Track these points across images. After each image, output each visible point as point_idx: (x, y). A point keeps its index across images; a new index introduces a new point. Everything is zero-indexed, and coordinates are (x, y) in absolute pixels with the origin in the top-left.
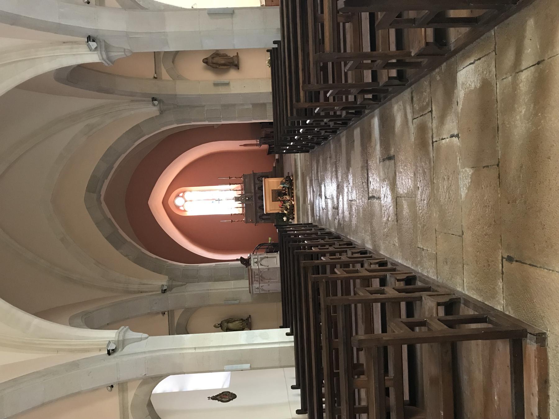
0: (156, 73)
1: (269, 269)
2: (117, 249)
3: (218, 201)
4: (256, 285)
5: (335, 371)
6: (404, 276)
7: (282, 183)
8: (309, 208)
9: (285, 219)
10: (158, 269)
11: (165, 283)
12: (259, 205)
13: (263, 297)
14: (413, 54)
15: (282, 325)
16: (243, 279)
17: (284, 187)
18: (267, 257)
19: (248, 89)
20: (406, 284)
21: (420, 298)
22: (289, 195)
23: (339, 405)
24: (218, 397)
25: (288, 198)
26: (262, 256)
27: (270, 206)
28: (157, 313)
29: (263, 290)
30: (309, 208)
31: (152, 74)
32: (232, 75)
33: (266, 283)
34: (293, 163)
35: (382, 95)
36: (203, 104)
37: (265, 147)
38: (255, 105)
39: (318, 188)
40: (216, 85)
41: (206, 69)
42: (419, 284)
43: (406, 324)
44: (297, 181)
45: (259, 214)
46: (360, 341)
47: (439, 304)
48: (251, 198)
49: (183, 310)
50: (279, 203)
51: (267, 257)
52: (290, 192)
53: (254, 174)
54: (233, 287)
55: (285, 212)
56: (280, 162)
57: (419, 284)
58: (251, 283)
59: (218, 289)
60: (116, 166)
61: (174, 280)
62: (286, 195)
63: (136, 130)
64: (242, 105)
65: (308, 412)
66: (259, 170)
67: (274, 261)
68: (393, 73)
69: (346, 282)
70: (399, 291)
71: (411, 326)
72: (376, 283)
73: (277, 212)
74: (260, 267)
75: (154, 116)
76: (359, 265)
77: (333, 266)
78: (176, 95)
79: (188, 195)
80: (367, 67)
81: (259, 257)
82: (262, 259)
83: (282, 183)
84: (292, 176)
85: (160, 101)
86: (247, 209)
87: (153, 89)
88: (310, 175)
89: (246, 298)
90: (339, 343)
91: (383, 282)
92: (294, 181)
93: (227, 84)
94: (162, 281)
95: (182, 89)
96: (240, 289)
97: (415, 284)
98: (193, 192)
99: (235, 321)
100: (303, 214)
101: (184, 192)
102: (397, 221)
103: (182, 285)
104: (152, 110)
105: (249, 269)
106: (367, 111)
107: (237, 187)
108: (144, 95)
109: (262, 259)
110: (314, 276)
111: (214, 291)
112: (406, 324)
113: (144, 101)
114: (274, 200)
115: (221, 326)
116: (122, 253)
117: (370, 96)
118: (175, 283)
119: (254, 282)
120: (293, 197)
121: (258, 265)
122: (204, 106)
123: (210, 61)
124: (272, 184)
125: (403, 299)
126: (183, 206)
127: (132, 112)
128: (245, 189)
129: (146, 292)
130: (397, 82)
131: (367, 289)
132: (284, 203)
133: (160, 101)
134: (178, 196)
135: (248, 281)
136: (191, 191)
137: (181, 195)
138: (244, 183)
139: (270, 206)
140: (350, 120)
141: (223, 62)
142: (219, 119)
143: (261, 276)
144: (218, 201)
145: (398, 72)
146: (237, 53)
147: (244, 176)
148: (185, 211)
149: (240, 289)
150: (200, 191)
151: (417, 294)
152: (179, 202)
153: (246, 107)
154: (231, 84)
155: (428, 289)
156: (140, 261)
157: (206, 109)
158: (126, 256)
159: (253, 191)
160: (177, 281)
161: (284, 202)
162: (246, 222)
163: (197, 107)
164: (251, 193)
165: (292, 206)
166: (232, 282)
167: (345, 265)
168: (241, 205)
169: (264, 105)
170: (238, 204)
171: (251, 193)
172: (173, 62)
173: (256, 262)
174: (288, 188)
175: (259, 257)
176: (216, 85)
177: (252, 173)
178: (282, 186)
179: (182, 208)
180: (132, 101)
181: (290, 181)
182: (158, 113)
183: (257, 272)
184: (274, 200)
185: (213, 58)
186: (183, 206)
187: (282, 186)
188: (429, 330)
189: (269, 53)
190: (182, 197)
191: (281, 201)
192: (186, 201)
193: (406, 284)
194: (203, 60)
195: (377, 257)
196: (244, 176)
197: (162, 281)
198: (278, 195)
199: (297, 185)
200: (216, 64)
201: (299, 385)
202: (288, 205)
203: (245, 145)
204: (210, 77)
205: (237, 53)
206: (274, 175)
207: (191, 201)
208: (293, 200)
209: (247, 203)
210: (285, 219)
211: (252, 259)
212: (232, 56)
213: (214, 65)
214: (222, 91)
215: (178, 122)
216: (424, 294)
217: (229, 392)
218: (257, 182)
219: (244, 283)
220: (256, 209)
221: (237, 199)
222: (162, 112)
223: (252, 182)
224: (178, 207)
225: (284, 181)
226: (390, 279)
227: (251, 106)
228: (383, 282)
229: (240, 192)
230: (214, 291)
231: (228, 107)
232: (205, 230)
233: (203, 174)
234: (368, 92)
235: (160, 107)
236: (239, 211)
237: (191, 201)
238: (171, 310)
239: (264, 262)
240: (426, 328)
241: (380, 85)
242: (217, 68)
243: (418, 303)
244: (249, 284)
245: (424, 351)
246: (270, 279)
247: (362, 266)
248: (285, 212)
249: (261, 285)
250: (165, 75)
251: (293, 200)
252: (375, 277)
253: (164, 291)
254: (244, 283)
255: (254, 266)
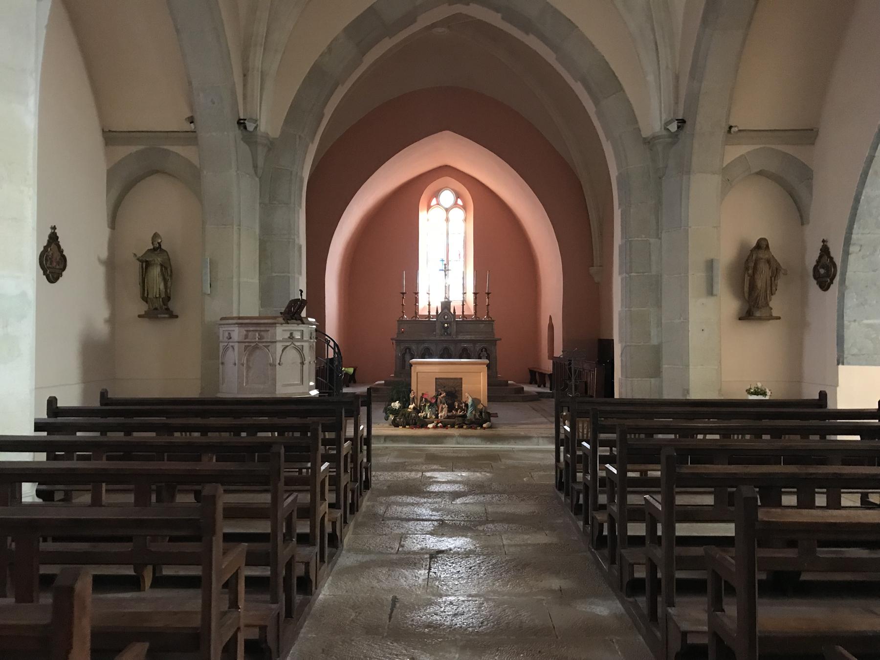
0: (740, 131)
1: (273, 365)
2: (346, 30)
3: (445, 267)
4: (237, 333)
5: (166, 454)
6: (313, 577)
7: (476, 402)
8: (413, 475)
9: (396, 405)
10: (297, 114)
11: (263, 127)
12: (433, 347)
13: (212, 351)
14: (670, 610)
15: (60, 404)
16: (263, 305)
17: (467, 405)
18: (302, 363)
19: (696, 339)
20: (299, 578)
21: (275, 601)
22: (448, 417)
23: (109, 458)
24: (53, 246)
25: (443, 414)
26: (306, 351)
27: (427, 372)
28: (191, 106)
29: (226, 349)
30: (413, 475)
31: (740, 121)
32: (728, 304)
33: (240, 359)
34: (520, 430)
35: (606, 552)
36: (664, 235)
37: (548, 366)
38: (657, 350)
39: (460, 520)
40: (710, 265)
41: (743, 246)
42: (298, 598)
43: (236, 575)
44: (479, 441)
45: (414, 347)
46: (213, 499)
47: (263, 628)
48: (448, 335)
49: (198, 166)
50: (431, 392)
51: (302, 363)
52: (456, 420)
53: (494, 342)
54: (242, 280)
55: (411, 406)
56: (518, 396)
57: (298, 598)
58: (242, 322)
59: (239, 245)
60: (532, 42)
61: (270, 150)
62: (450, 410)
63: (608, 84)
64: (659, 324)
65: (52, 420)
66: (501, 350)
67: (296, 381)
68: (640, 573)
69: (307, 482)
70: (289, 566)
71: (230, 585)
72: (303, 528)
73: (413, 387)
74: (279, 347)
75: (641, 124)
76: (334, 501)
77: (334, 460)
78: (688, 173)
79: (458, 214)
80: (652, 529)
81: (306, 345)
82: (300, 350)
83: (476, 402)
84: (490, 427)
85: (675, 137)
86: (427, 323)
87: (706, 121)
88: (495, 486)
89: (215, 309)
90: (210, 463)
91: (305, 540)
92: (479, 431)
93: (710, 291)
94: (269, 121)
95: (703, 187)
96: (235, 298)
97: (298, 593)
98: (462, 224)
99: (165, 281)
100: (402, 453)
101: (464, 207)
102: (390, 618)
103: (255, 167)
104: (654, 118)
105: (275, 318)
106: (581, 523)
107: (469, 308)
108: (693, 100)
109: (300, 350)
110: (283, 450)
111: (235, 236)
112: (236, 575)
113: (677, 103)
114: (440, 383)
115: (155, 249)
116: (336, 39)
117: (581, 501)
118: (261, 152)
119: (243, 331)
120: (445, 426)
121: (284, 341)
122: (658, 237)
123: (762, 255)
124: (474, 379)
125: (275, 572)
126: (438, 204)
127: (651, 78)
128: (465, 321)
129: (245, 85)
130: (626, 579)
131: (295, 514)
132: (431, 405)
133: (675, 137)
134: (458, 196)
135: (257, 315)
136: (465, 220)
137: (460, 202)
138: (477, 321)
139: (427, 372)
140: (567, 495)
141: (760, 283)
142: (628, 268)
143: (256, 348)
144: (445, 267)
145: (642, 580)
146: (779, 318)
147: (490, 322)
148: (429, 207)
149: (235, 298)
150: (464, 273)
151: (282, 597)
152: (447, 197)
153: (654, 332)
154: (710, 301)
155: (289, 613)
156: (318, 79)
157: (652, 240)
158: (330, 49)
159: (460, 338)
160: (265, 157)
161: (434, 405)
162: (401, 322)
163: (657, 223)
164: (457, 333)
165: (423, 424)
166: (256, 281)
167: (335, 481)
168: (433, 313)
169: (656, 371)
170: (436, 305)
171: (457, 333)
172: (760, 173)
173: (291, 337)
174: (464, 416)
175: (306, 345)
176: (710, 265)
177: (496, 337)
178: (470, 402)
179: (434, 201)
180: (677, 78)
181: (481, 419)
182: (646, 133)
183: (268, 337)
184: (440, 383)
185: (768, 261)
186: (438, 204)
187: (470, 402)
188: (224, 614)
189: (817, 397)
190: (456, 204)
191: (436, 397)
192: (447, 210)
193: (299, 578)
194: (765, 239)
195: (320, 573)
196: (490, 322)
197: (269, 121)
198: (450, 391)
199: (470, 440)
200: (755, 269)
201: (106, 405)
202: (428, 413)
203: (551, 327)
204: (726, 254)
205: (779, 318)
206: (494, 383)
207: (447, 220)
208: (436, 427)
209: (438, 326)
210: (396, 405)
211: (302, 327)
212: (771, 304)
213: (752, 265)
214: (696, 278)
215: (623, 180)
216: (280, 607)
217: (64, 269)
218: (478, 347)
219: (249, 304)
220: (424, 341)
221: (446, 305)
222: (649, 142)
223: (479, 337)
224: (436, 194)
225: (480, 407)
226: (310, 552)
227: (654, 341)
228: (305, 540)
229: (459, 312)
230: (235, 236)
231: (652, 289)
232: (390, 238)
233: (498, 243)
234: (612, 529)
235: (658, 137)
236: (424, 309)
237: (447, 220)
238: (196, 137)
239: (292, 355)
240: (226, 609)
241: (623, 551)
242: (747, 269)
243: (268, 597)
244: (239, 318)
245: (188, 601)
246: (249, 368)
247: (331, 506)
248: (411, 406)
249: (236, 345)
250: (735, 152)
251: (436, 427)
252: (313, 527)
253: (241, 123)
254: (249, 304)
255: (281, 332)
